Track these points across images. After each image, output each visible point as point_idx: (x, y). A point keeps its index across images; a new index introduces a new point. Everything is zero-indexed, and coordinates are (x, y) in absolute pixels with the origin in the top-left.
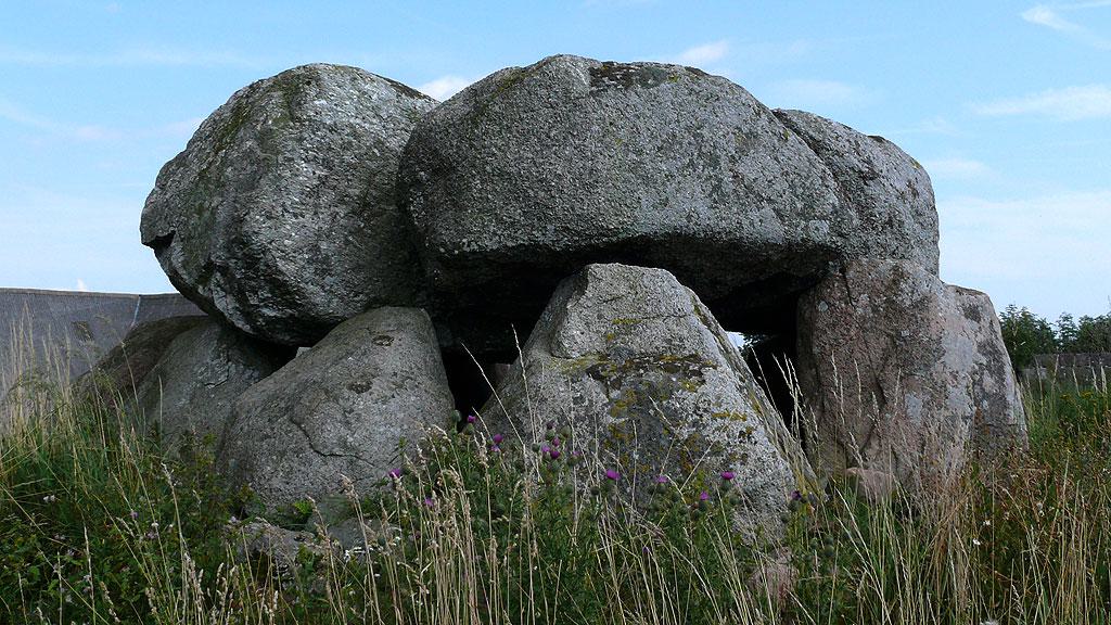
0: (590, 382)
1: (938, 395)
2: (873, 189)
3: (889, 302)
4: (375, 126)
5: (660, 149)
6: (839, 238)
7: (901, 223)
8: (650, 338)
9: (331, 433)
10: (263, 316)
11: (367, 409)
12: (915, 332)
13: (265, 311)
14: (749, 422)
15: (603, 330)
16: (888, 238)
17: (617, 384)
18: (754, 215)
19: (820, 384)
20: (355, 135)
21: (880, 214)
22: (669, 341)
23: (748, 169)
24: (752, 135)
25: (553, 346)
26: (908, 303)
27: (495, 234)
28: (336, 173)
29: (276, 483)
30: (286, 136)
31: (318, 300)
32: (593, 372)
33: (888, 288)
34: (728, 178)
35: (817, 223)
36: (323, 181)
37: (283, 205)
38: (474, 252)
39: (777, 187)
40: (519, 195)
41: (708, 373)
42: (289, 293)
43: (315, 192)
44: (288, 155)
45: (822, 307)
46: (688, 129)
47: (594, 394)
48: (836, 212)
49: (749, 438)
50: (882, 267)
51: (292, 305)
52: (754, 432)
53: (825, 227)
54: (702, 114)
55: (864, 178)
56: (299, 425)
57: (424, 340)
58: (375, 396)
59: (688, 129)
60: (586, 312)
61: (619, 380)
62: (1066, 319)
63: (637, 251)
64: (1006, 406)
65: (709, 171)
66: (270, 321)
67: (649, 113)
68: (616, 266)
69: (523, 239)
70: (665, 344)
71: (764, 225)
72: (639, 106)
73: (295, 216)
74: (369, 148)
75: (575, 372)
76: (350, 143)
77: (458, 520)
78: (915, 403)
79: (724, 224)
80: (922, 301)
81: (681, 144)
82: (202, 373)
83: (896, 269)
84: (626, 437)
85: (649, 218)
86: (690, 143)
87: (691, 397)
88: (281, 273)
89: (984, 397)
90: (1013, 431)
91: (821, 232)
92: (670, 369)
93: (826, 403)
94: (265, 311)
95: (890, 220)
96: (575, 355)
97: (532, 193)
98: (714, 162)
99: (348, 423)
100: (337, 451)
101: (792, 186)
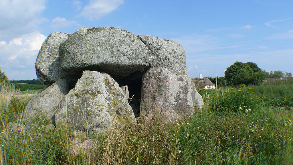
1: (166, 99)
2: (160, 51)
3: (158, 77)
5: (99, 45)
6: (146, 63)
7: (169, 59)
11: (41, 101)
12: (163, 84)
13: (43, 80)
15: (84, 85)
18: (122, 59)
21: (162, 57)
23: (121, 49)
26: (162, 78)
28: (53, 53)
31: (51, 78)
33: (159, 74)
34: (116, 51)
35: (139, 60)
36: (50, 55)
37: (42, 60)
41: (99, 95)
42: (45, 77)
43: (49, 57)
44: (44, 51)
45: (145, 79)
46: (106, 41)
47: (75, 99)
48: (145, 57)
50: (157, 70)
51: (47, 79)
52: (103, 110)
53: (141, 61)
54: (110, 37)
55: (157, 49)
58: (44, 98)
59: (106, 41)
62: (272, 72)
63: (101, 68)
64: (187, 101)
68: (88, 71)
71: (125, 61)
72: (95, 36)
73: (45, 62)
76: (56, 47)
77: (211, 96)
78: (161, 101)
79: (114, 61)
80: (165, 77)
81: (104, 44)
83: (160, 70)
84: (78, 109)
85: (95, 60)
86: (107, 44)
88: (42, 73)
89: (179, 99)
90: (188, 107)
92: (91, 94)
93: (144, 100)
94: (43, 80)
96: (77, 90)
98: (113, 47)
101: (133, 52)
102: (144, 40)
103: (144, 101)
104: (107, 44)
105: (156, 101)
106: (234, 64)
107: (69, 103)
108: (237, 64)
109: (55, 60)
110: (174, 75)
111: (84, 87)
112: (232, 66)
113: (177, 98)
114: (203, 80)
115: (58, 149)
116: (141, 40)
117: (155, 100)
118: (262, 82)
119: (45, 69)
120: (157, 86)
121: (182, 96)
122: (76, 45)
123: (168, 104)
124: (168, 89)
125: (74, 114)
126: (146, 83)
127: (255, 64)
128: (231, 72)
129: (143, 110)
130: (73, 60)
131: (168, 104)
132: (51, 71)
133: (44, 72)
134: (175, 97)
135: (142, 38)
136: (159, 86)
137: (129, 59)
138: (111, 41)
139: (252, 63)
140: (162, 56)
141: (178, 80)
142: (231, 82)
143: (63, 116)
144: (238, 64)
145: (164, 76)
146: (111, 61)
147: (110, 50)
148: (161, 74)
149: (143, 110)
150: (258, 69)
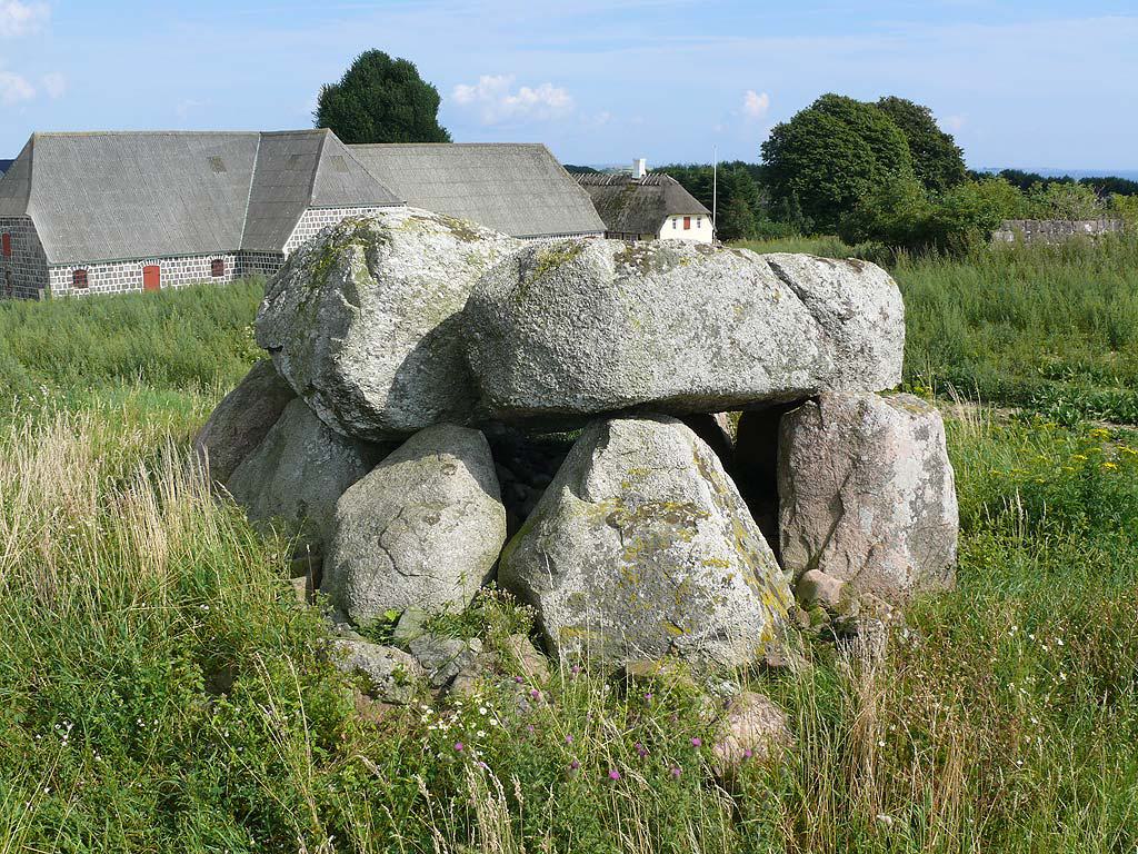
0: (608, 530)
1: (886, 510)
2: (849, 326)
3: (854, 430)
4: (439, 273)
8: (657, 487)
9: (410, 559)
10: (355, 428)
13: (357, 424)
14: (731, 570)
15: (621, 478)
16: (861, 363)
17: (630, 533)
18: (747, 374)
19: (793, 491)
20: (424, 284)
22: (672, 491)
23: (742, 336)
24: (750, 304)
25: (581, 492)
27: (535, 395)
29: (371, 595)
30: (366, 289)
32: (611, 522)
33: (854, 418)
34: (726, 345)
38: (519, 406)
39: (767, 347)
40: (551, 365)
41: (701, 524)
43: (392, 336)
44: (369, 308)
45: (799, 431)
49: (729, 584)
52: (733, 579)
53: (805, 375)
54: (707, 293)
56: (386, 549)
57: (482, 463)
58: (443, 527)
60: (607, 463)
61: (631, 529)
65: (711, 341)
66: (360, 430)
67: (662, 297)
69: (559, 403)
70: (669, 493)
73: (377, 357)
74: (435, 293)
75: (597, 521)
78: (868, 517)
82: (310, 449)
85: (659, 386)
86: (696, 319)
87: (686, 547)
91: (802, 380)
92: (672, 519)
93: (797, 506)
94: (357, 424)
95: (862, 349)
96: (598, 499)
97: (565, 367)
98: (716, 332)
99: (424, 550)
100: (415, 572)
102: (800, 284)
103: (794, 512)
104: (696, 319)
105: (847, 514)
106: (815, 108)
107: (593, 554)
108: (827, 110)
109: (413, 346)
110: (906, 419)
111: (623, 485)
112: (801, 119)
113: (919, 502)
114: (651, 189)
115: (59, 656)
116: (789, 284)
117: (843, 512)
118: (988, 237)
119: (381, 384)
120: (847, 461)
121: (930, 493)
122: (580, 324)
123: (892, 526)
124: (892, 474)
125: (624, 597)
126: (808, 447)
127: (920, 109)
128: (796, 150)
129: (795, 542)
130: (573, 386)
131: (892, 526)
132: (398, 390)
133: (377, 397)
134: (911, 503)
135: (792, 276)
136: (856, 462)
137: (769, 373)
138: (709, 308)
139: (907, 106)
140: (855, 343)
141: (917, 439)
142: (791, 201)
143: (576, 603)
144: (833, 106)
145: (876, 428)
146: (711, 384)
147: (708, 342)
148: (866, 418)
149: (795, 542)
150: (935, 137)
